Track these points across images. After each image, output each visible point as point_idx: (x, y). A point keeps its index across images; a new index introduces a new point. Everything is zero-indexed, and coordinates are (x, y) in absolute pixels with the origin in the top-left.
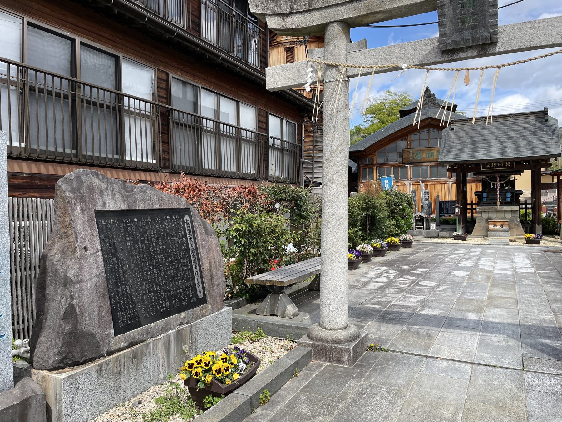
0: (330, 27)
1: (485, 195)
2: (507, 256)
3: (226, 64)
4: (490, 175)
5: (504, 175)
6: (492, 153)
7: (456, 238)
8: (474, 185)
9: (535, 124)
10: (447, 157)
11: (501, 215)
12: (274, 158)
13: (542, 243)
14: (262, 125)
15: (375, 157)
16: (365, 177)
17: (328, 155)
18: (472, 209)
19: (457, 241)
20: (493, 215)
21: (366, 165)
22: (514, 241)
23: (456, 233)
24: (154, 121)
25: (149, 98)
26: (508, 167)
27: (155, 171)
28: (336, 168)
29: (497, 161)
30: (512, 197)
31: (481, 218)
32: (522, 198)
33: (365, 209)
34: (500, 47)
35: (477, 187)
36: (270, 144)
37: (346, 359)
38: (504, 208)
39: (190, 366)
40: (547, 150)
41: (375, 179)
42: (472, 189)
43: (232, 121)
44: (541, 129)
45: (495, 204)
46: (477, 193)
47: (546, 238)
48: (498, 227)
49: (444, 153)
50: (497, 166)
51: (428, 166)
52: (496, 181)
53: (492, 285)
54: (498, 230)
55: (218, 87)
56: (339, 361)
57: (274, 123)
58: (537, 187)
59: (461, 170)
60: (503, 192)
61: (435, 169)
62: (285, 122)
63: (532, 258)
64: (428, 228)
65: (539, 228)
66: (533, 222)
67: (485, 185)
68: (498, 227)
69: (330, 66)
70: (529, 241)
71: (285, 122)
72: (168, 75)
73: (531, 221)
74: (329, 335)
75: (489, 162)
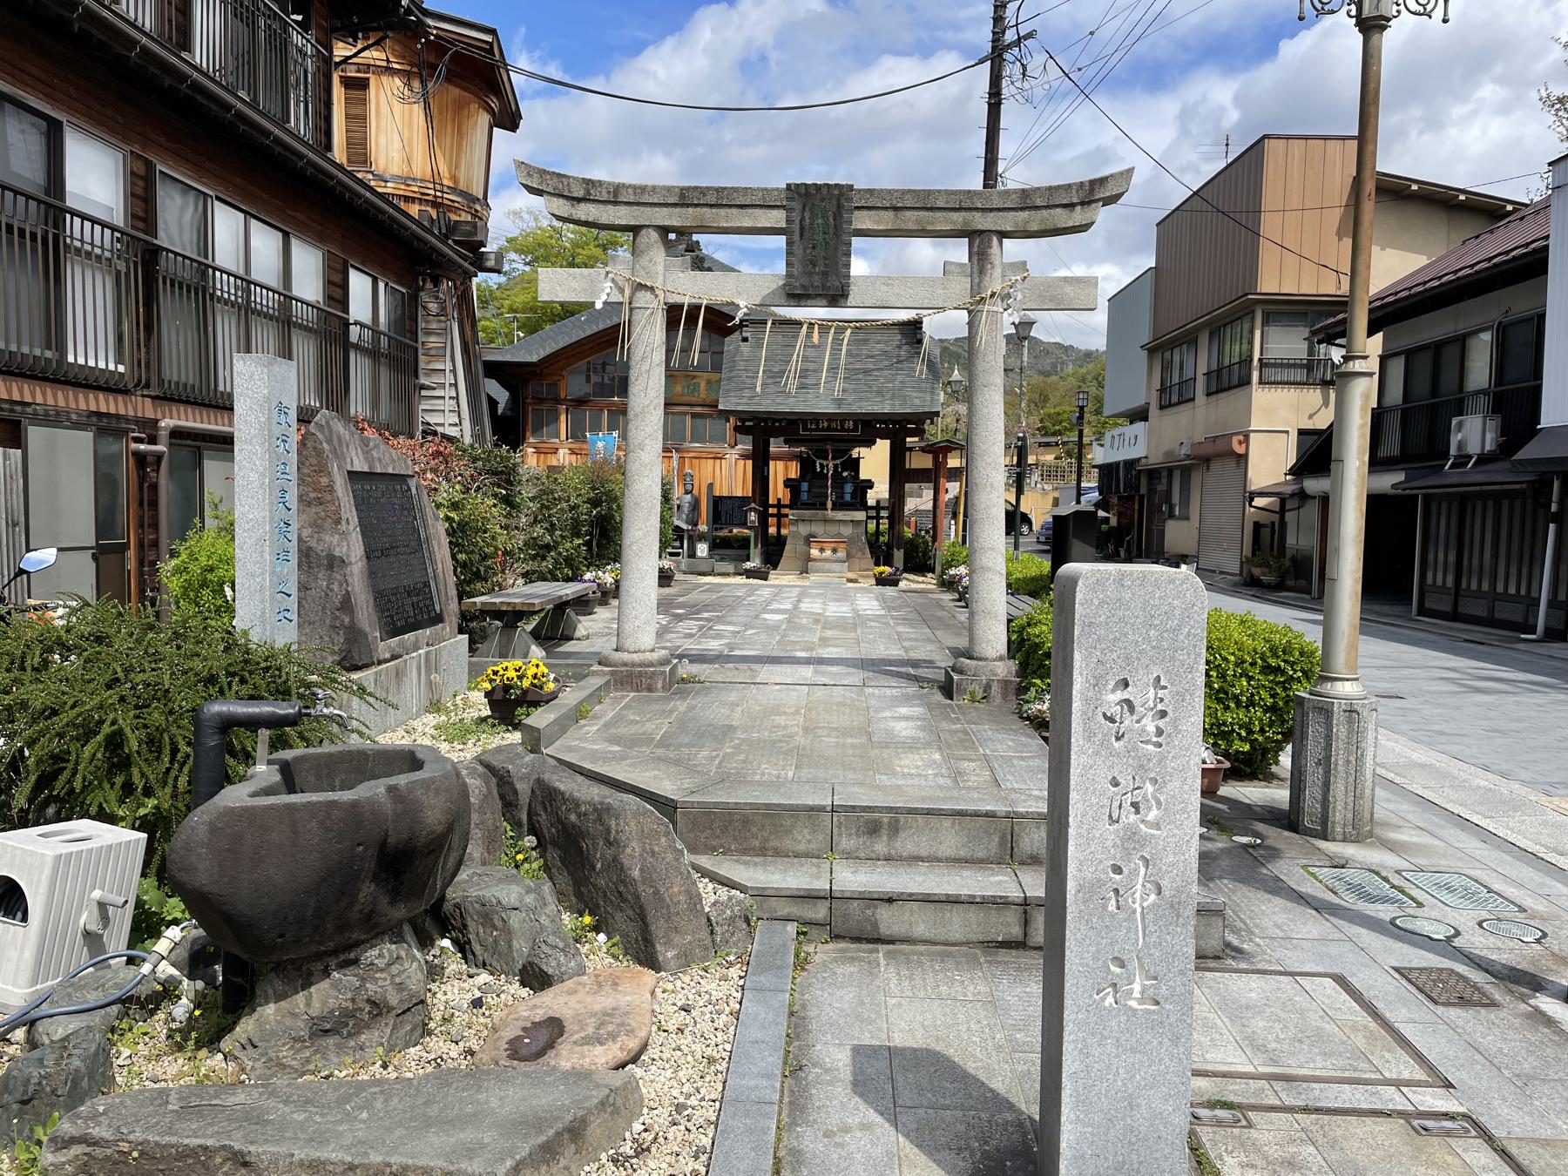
0: (644, 232)
1: (805, 486)
2: (844, 597)
3: (279, 149)
4: (816, 446)
5: (842, 446)
6: (824, 397)
7: (750, 574)
8: (780, 464)
9: (899, 347)
10: (734, 400)
11: (833, 529)
12: (359, 368)
13: (903, 584)
14: (337, 292)
15: (563, 383)
16: (537, 430)
17: (638, 410)
18: (779, 516)
19: (751, 581)
20: (817, 529)
21: (541, 401)
22: (855, 581)
23: (748, 565)
24: (118, 273)
25: (119, 219)
26: (849, 430)
27: (125, 392)
28: (649, 430)
29: (830, 417)
30: (853, 494)
31: (796, 535)
32: (872, 497)
33: (595, 503)
34: (851, 300)
35: (786, 468)
36: (354, 338)
37: (660, 685)
38: (840, 515)
39: (495, 673)
40: (917, 401)
41: (563, 436)
42: (781, 472)
43: (273, 280)
44: (910, 359)
45: (823, 507)
46: (788, 483)
47: (911, 577)
48: (828, 553)
49: (729, 391)
50: (829, 429)
51: (685, 414)
52: (826, 458)
53: (824, 628)
54: (826, 560)
55: (248, 197)
56: (650, 689)
57: (359, 284)
58: (900, 475)
59: (761, 430)
60: (839, 482)
61: (699, 421)
62: (381, 286)
63: (883, 600)
64: (692, 555)
65: (899, 555)
66: (890, 546)
67: (806, 465)
68: (828, 553)
69: (642, 287)
70: (881, 581)
71: (381, 286)
72: (149, 165)
73: (887, 544)
74: (636, 657)
75: (816, 418)
